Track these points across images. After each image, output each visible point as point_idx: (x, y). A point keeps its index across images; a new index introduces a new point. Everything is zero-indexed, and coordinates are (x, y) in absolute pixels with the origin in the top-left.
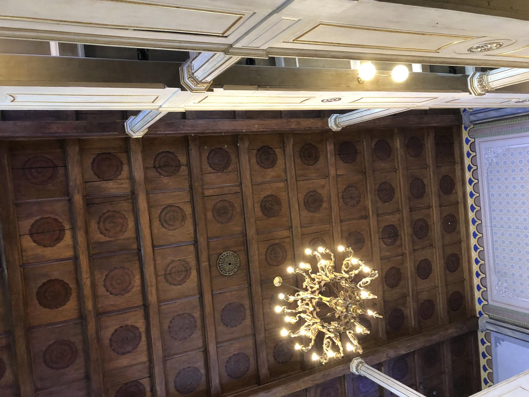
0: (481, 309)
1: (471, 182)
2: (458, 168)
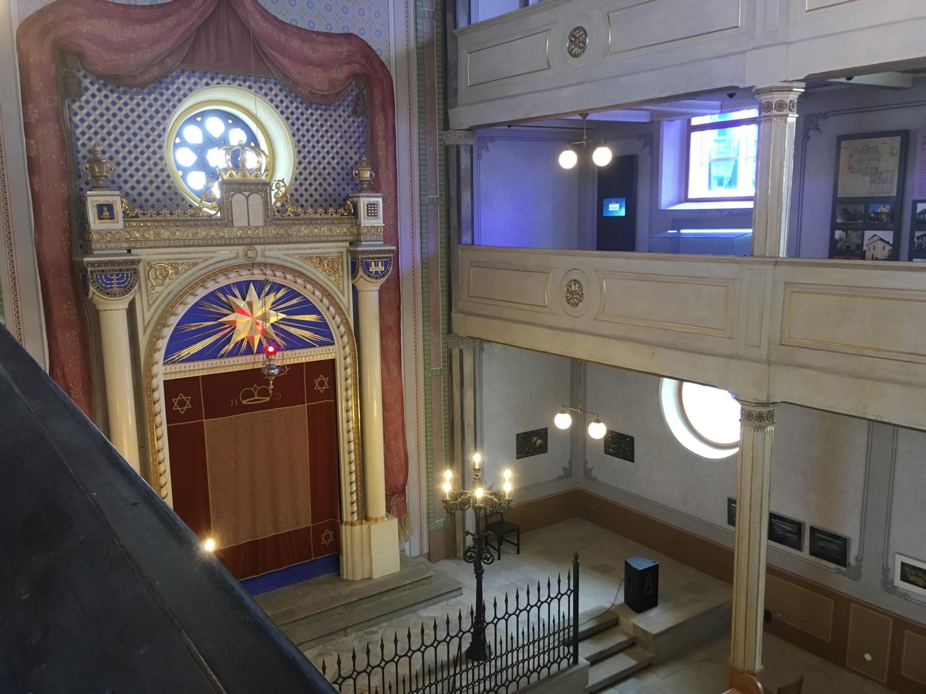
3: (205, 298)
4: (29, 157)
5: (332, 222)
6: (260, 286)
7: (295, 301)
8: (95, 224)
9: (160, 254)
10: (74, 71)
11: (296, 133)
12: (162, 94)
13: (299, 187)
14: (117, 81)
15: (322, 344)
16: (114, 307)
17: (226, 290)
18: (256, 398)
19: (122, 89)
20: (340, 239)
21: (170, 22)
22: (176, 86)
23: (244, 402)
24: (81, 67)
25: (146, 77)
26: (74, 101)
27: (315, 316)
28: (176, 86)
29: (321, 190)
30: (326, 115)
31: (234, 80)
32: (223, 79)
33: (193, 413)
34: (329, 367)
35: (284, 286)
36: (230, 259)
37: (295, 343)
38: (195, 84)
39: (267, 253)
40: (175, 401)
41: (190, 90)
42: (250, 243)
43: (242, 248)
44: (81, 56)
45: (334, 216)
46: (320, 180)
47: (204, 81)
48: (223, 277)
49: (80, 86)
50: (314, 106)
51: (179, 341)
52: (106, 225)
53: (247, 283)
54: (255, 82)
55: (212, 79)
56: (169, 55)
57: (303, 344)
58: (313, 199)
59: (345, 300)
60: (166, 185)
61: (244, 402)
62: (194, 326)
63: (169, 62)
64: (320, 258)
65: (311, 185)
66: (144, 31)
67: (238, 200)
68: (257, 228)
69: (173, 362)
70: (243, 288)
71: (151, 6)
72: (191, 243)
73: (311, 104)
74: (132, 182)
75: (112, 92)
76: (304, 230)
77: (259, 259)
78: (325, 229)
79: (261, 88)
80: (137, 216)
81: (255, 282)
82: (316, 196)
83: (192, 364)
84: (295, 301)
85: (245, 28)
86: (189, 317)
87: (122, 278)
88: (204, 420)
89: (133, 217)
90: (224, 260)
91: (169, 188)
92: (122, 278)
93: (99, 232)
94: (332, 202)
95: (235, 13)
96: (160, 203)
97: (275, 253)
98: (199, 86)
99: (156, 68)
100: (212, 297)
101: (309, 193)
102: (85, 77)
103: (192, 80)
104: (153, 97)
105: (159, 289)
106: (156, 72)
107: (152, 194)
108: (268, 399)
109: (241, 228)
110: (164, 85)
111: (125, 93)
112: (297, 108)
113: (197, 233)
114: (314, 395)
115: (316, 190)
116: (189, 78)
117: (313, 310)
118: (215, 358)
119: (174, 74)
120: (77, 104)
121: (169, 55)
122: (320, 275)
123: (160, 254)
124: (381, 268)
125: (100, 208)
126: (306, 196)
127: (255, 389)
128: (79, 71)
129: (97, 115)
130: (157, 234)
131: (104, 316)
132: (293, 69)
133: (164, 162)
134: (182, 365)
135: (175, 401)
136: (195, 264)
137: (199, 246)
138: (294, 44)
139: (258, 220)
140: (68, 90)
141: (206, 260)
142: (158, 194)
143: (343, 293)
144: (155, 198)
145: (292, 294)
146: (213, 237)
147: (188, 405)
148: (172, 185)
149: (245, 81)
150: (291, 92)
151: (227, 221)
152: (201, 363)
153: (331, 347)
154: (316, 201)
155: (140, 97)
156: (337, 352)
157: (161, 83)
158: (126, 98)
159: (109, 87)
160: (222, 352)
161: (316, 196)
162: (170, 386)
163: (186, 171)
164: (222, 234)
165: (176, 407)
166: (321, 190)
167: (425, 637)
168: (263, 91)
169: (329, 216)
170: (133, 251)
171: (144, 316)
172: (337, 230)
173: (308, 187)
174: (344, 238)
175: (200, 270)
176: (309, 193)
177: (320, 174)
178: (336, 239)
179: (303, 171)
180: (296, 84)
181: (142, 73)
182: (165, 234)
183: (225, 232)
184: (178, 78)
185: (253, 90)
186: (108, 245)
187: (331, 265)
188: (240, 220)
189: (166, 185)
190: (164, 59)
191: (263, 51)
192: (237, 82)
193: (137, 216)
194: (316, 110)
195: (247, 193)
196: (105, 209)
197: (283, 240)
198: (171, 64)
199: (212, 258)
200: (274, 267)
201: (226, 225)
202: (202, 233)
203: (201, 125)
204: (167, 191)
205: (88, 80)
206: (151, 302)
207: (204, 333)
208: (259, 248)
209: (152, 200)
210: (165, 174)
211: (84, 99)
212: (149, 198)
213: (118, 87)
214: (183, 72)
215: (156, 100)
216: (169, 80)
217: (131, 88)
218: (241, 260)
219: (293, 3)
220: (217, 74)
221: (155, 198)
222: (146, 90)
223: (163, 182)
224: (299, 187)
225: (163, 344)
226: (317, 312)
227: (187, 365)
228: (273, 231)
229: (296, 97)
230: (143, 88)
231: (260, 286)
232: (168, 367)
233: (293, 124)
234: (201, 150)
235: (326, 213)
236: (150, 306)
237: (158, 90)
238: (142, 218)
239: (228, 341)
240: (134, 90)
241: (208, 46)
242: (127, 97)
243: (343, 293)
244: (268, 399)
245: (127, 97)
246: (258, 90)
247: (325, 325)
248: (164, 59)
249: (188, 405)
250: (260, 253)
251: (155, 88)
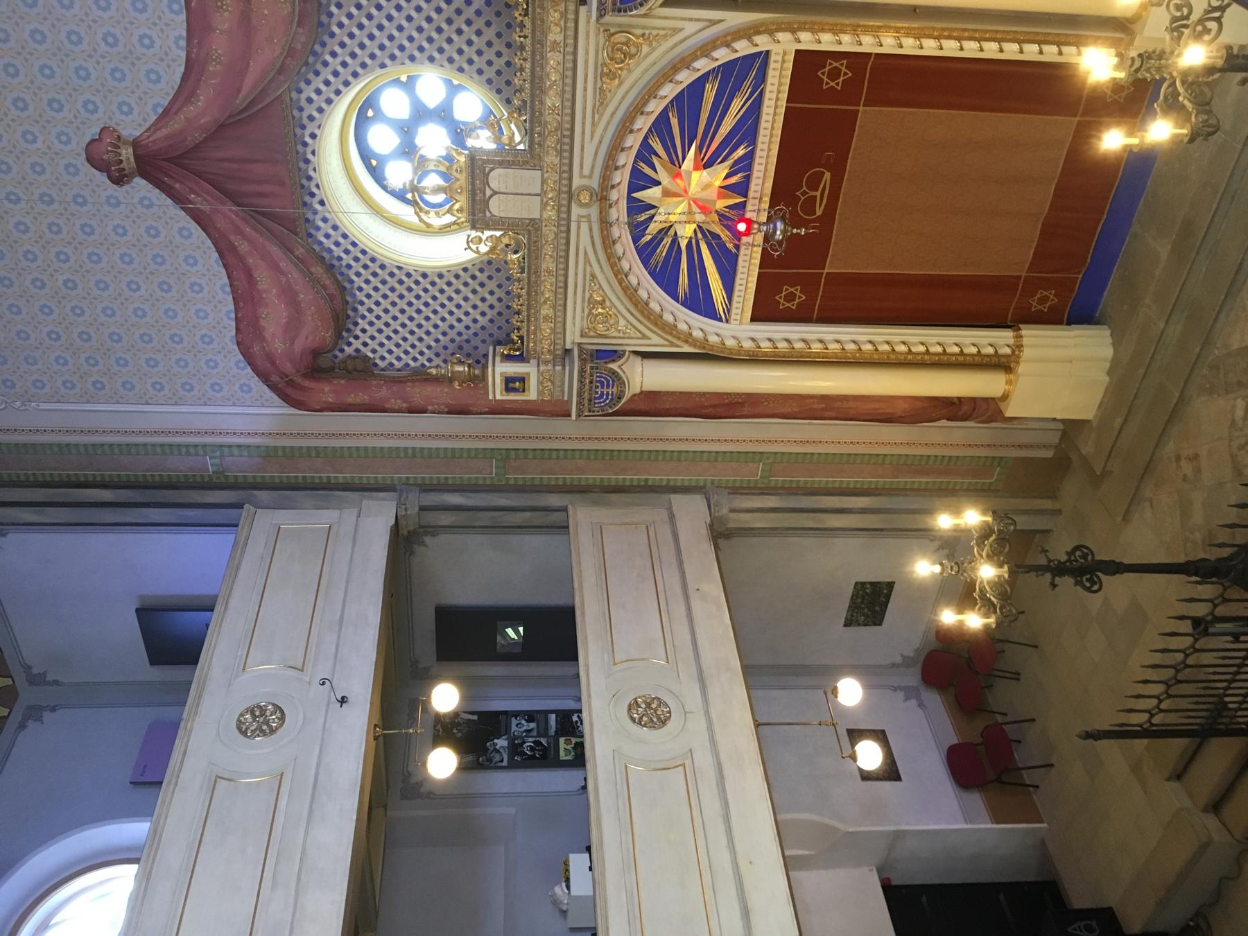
3: (645, 262)
4: (448, 413)
5: (539, 42)
6: (640, 181)
7: (674, 122)
8: (532, 394)
9: (574, 318)
10: (337, 361)
11: (378, 61)
12: (349, 267)
13: (475, 67)
14: (341, 316)
15: (762, 77)
16: (639, 385)
17: (637, 231)
18: (818, 194)
19: (350, 312)
20: (571, 25)
21: (244, 247)
22: (333, 247)
23: (819, 213)
24: (329, 355)
25: (328, 282)
26: (376, 365)
27: (708, 86)
28: (333, 247)
29: (479, 23)
31: (307, 161)
32: (310, 178)
33: (809, 284)
34: (806, 62)
35: (646, 138)
36: (591, 230)
37: (747, 130)
38: (325, 220)
39: (586, 171)
40: (783, 304)
41: (335, 228)
42: (569, 196)
43: (574, 206)
44: (316, 353)
45: (527, 31)
46: (460, 22)
47: (318, 207)
48: (618, 173)
49: (355, 358)
50: (324, 19)
51: (700, 302)
52: (533, 383)
53: (630, 200)
54: (303, 127)
55: (313, 195)
56: (292, 252)
57: (754, 111)
58: (495, 40)
59: (691, 28)
60: (478, 274)
61: (819, 213)
62: (683, 279)
63: (300, 251)
64: (602, 75)
65: (470, 43)
66: (264, 279)
67: (497, 207)
68: (544, 181)
69: (728, 310)
70: (637, 207)
71: (225, 266)
72: (561, 278)
73: (321, 24)
74: (475, 314)
75: (356, 324)
76: (552, 100)
77: (595, 183)
78: (553, 59)
79: (311, 118)
80: (521, 338)
81: (633, 188)
82: (490, 33)
83: (736, 293)
84: (674, 122)
85: (221, 130)
86: (672, 291)
87: (602, 383)
88: (826, 271)
89: (522, 343)
90: (592, 237)
91: (481, 270)
92: (602, 383)
93: (540, 393)
94: (503, 79)
95: (197, 146)
96: (500, 306)
97: (585, 173)
98: (327, 215)
99: (313, 270)
100: (646, 253)
101: (484, 48)
102: (342, 351)
103: (321, 224)
104: (354, 278)
105: (622, 322)
106: (318, 270)
107: (492, 293)
108: (827, 175)
109: (544, 206)
110: (335, 262)
111: (355, 310)
112: (334, 54)
113: (549, 272)
114: (851, 93)
115: (479, 33)
116: (318, 229)
117: (697, 88)
118: (737, 256)
119: (316, 247)
120: (378, 361)
121: (292, 252)
122: (637, 74)
123: (574, 318)
125: (508, 390)
126: (490, 54)
127: (804, 193)
128: (336, 357)
129: (380, 338)
130: (546, 319)
131: (646, 388)
132: (265, 56)
133: (445, 274)
134: (735, 305)
135: (783, 304)
136: (593, 276)
137: (566, 269)
138: (220, 45)
139: (530, 179)
140: (361, 369)
141: (593, 124)
142: (492, 285)
143: (676, 31)
144: (496, 290)
145: (661, 126)
146: (556, 249)
147: (797, 290)
148: (478, 267)
149: (305, 144)
150: (307, 64)
151: (532, 227)
152: (739, 276)
153: (773, 58)
154: (500, 286)
155: (358, 293)
156: (782, 48)
157: (333, 266)
158: (362, 310)
159: (351, 327)
160: (730, 246)
161: (490, 33)
162: (758, 316)
163: (453, 89)
164: (552, 236)
165: (832, 64)
166: (479, 23)
167: (1181, 631)
168: (315, 114)
169: (527, 22)
170: (568, 347)
171: (656, 342)
172: (555, 35)
173: (479, 311)
174: (571, 16)
175: (603, 271)
176: (484, 48)
177: (449, 21)
178: (571, 33)
179: (446, 55)
180: (291, 53)
181: (324, 287)
182: (546, 311)
183: (549, 232)
184: (321, 243)
185: (317, 132)
186: (558, 383)
187: (621, 53)
188: (530, 209)
189: (478, 274)
190: (297, 258)
191: (245, 109)
192: (310, 156)
193: (521, 338)
194: (330, 15)
195: (488, 193)
196: (511, 385)
197: (567, 140)
198: (302, 250)
199: (586, 253)
200: (610, 166)
201: (538, 229)
202: (548, 264)
203: (379, 116)
204: (486, 274)
205: (346, 348)
206: (639, 335)
207: (697, 268)
208: (577, 182)
209: (500, 293)
210: (461, 273)
211: (371, 355)
212: (496, 296)
213: (348, 317)
214: (310, 235)
215: (358, 274)
216: (325, 254)
217: (347, 302)
218: (594, 211)
219: (139, 5)
220: (302, 186)
221: (496, 290)
222: (347, 285)
223: (474, 277)
224: (475, 67)
226: (704, 79)
227: (735, 299)
228: (551, 159)
229: (315, 54)
230: (345, 288)
231: (640, 181)
232: (733, 317)
233: (364, 65)
234: (421, 114)
235: (522, 48)
236: (644, 337)
237: (344, 270)
238: (524, 332)
239: (716, 236)
240: (349, 299)
241: (261, 195)
242: (360, 307)
243: (676, 31)
244: (827, 175)
245: (360, 307)
246: (316, 123)
247: (728, 67)
248: (297, 258)
249: (797, 290)
250: (585, 182)
251: (342, 274)
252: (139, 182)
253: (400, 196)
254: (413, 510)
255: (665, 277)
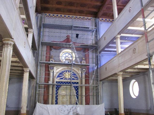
0: (66, 16)
1: (69, 17)
2: (85, 15)
14: (55, 49)
15: (77, 80)
30: (79, 52)
37: (73, 79)
51: (58, 76)
57: (74, 79)
70: (67, 71)
124: (85, 70)
140: (51, 50)
207: (61, 76)
225: (57, 76)
247: (77, 77)
252: (66, 38)
253: (63, 55)
254: (37, 52)
255: (60, 74)
